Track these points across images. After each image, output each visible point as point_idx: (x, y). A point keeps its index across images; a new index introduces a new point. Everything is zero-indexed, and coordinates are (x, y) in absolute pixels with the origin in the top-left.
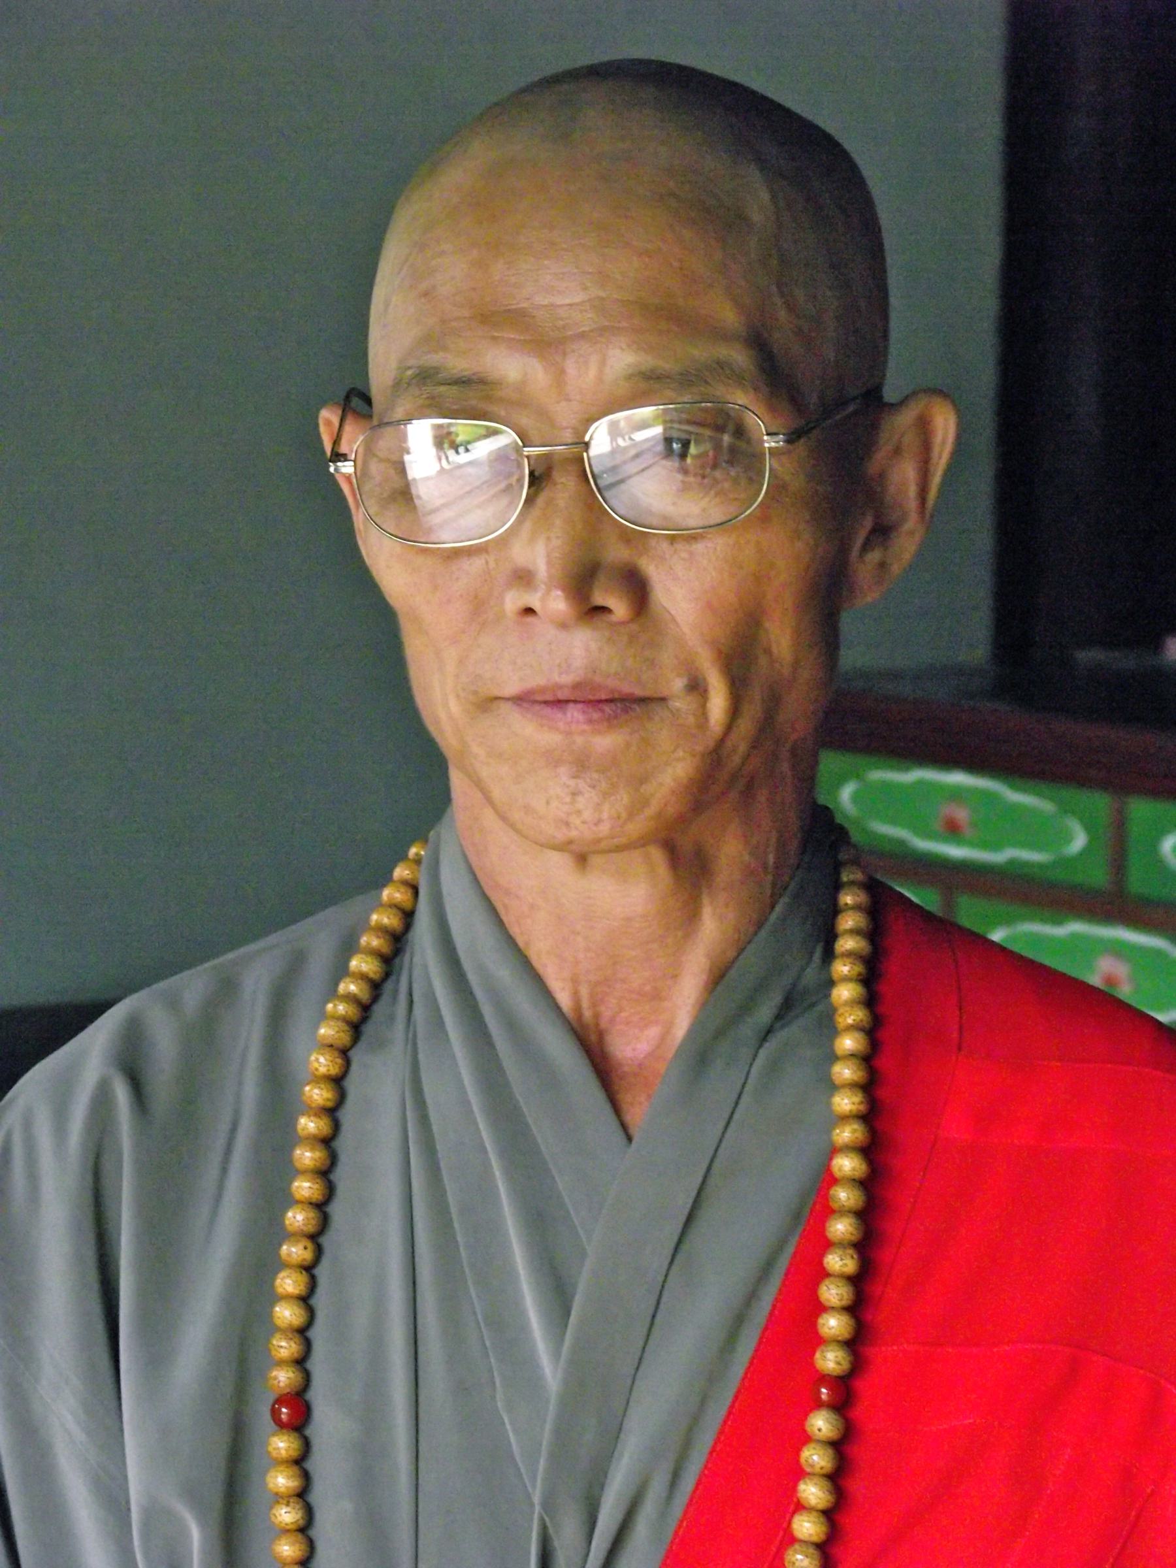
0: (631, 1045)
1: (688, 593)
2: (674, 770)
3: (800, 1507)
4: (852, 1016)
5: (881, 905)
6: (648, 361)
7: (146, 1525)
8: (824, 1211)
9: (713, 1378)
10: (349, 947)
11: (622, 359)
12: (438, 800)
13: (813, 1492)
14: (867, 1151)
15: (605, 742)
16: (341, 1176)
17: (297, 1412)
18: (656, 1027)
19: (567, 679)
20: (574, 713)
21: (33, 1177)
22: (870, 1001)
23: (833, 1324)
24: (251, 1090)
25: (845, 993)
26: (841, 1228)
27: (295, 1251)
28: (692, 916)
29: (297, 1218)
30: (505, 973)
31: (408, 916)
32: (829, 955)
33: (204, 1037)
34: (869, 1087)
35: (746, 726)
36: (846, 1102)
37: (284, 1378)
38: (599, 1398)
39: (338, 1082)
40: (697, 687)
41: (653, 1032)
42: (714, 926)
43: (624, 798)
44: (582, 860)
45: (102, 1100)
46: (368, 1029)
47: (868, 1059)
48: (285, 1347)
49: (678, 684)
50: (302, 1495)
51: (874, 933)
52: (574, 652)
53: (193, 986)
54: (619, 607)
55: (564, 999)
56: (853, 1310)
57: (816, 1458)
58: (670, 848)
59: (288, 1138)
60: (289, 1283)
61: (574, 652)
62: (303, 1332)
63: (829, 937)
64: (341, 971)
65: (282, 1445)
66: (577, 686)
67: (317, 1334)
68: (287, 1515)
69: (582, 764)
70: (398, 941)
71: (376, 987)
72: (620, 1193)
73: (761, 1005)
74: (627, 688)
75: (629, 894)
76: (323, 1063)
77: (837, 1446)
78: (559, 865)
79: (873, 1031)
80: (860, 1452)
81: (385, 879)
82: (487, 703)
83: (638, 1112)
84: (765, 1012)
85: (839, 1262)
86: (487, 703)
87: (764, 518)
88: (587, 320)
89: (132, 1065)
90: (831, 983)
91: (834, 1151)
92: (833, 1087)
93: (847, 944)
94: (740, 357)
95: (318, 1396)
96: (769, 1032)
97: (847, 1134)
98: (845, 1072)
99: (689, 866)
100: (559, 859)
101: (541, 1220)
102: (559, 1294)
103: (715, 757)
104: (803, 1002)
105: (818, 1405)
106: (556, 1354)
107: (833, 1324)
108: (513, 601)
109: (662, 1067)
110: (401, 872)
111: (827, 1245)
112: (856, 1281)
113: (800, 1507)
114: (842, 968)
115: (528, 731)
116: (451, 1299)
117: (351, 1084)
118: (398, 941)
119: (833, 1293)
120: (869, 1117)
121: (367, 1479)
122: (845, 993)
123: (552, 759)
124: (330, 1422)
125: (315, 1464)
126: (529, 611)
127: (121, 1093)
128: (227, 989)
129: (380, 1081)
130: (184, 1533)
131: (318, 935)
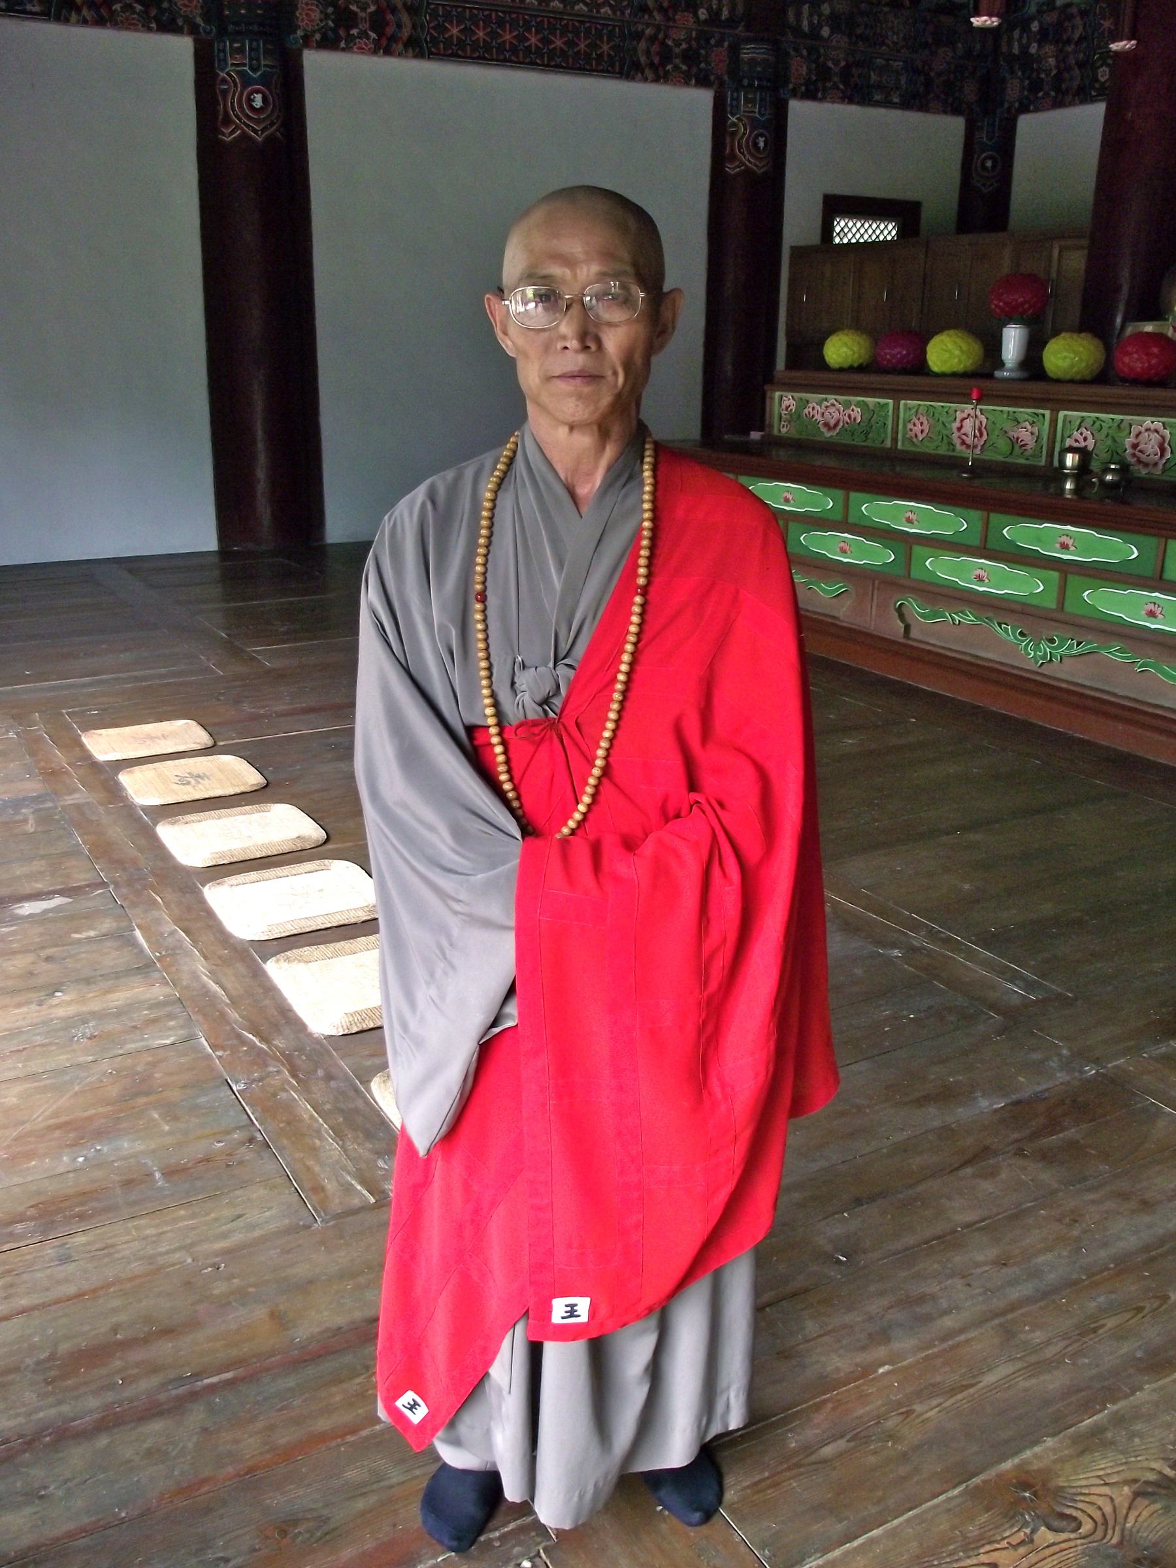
0: (583, 490)
1: (614, 342)
2: (606, 400)
3: (631, 623)
4: (649, 481)
5: (658, 447)
6: (605, 269)
7: (439, 629)
8: (640, 538)
9: (603, 592)
10: (497, 461)
11: (595, 268)
12: (522, 417)
13: (635, 619)
14: (653, 520)
15: (587, 390)
16: (495, 529)
17: (483, 597)
18: (588, 488)
19: (577, 369)
20: (578, 380)
21: (403, 530)
22: (655, 476)
23: (642, 571)
24: (467, 506)
25: (647, 474)
26: (645, 543)
27: (481, 551)
28: (603, 448)
29: (482, 541)
30: (544, 468)
31: (515, 452)
32: (642, 463)
33: (454, 489)
34: (654, 501)
35: (627, 388)
36: (646, 506)
37: (479, 587)
38: (572, 590)
39: (494, 501)
40: (615, 373)
41: (589, 486)
42: (610, 452)
43: (592, 408)
44: (572, 428)
45: (423, 505)
46: (503, 486)
47: (654, 493)
48: (479, 578)
49: (610, 373)
50: (484, 620)
51: (656, 456)
52: (576, 361)
53: (450, 475)
54: (593, 347)
55: (562, 476)
56: (648, 566)
57: (636, 609)
58: (600, 426)
59: (480, 518)
60: (479, 560)
61: (576, 361)
62: (484, 574)
63: (642, 458)
64: (495, 469)
65: (478, 606)
66: (580, 371)
67: (488, 575)
68: (480, 626)
69: (580, 397)
70: (511, 461)
71: (505, 473)
72: (578, 532)
73: (622, 475)
74: (596, 373)
75: (585, 440)
76: (489, 495)
77: (643, 606)
78: (563, 431)
79: (655, 485)
80: (649, 608)
81: (508, 442)
82: (549, 379)
83: (584, 510)
84: (623, 480)
85: (644, 553)
86: (549, 379)
87: (637, 321)
88: (581, 257)
89: (432, 496)
90: (642, 471)
91: (643, 520)
92: (643, 502)
93: (647, 460)
94: (628, 268)
95: (489, 593)
96: (624, 485)
97: (647, 515)
98: (646, 497)
99: (603, 433)
100: (561, 431)
101: (555, 541)
102: (560, 565)
103: (619, 396)
104: (633, 476)
105: (637, 594)
106: (559, 579)
107: (642, 571)
108: (559, 346)
109: (591, 496)
110: (512, 440)
111: (641, 548)
112: (649, 558)
113: (631, 623)
114: (646, 467)
115: (562, 386)
116: (528, 564)
117: (498, 502)
118: (511, 461)
119: (642, 562)
120: (654, 510)
121: (504, 618)
122: (647, 474)
123: (570, 395)
124: (492, 600)
125: (488, 612)
126: (566, 348)
127: (429, 506)
128: (458, 479)
129: (506, 501)
130: (450, 631)
131: (488, 458)
